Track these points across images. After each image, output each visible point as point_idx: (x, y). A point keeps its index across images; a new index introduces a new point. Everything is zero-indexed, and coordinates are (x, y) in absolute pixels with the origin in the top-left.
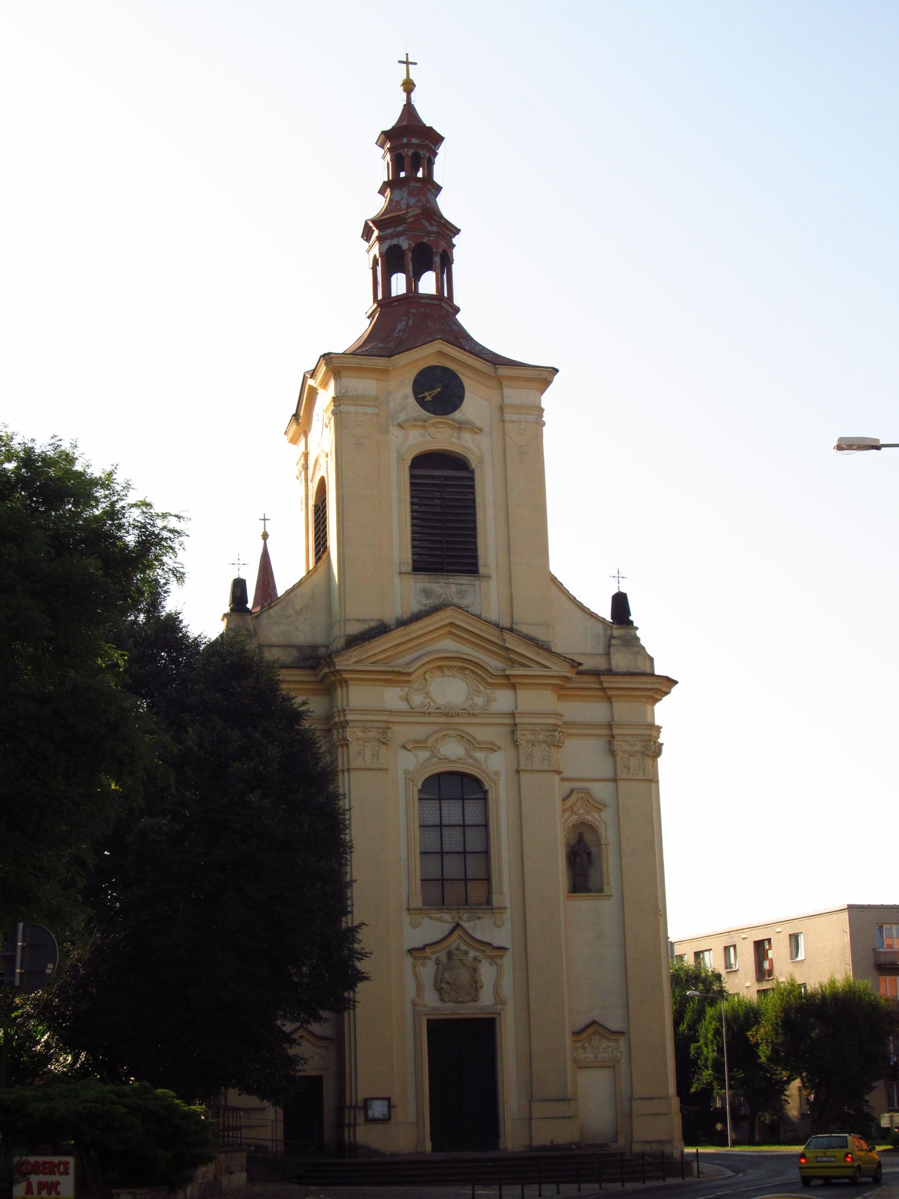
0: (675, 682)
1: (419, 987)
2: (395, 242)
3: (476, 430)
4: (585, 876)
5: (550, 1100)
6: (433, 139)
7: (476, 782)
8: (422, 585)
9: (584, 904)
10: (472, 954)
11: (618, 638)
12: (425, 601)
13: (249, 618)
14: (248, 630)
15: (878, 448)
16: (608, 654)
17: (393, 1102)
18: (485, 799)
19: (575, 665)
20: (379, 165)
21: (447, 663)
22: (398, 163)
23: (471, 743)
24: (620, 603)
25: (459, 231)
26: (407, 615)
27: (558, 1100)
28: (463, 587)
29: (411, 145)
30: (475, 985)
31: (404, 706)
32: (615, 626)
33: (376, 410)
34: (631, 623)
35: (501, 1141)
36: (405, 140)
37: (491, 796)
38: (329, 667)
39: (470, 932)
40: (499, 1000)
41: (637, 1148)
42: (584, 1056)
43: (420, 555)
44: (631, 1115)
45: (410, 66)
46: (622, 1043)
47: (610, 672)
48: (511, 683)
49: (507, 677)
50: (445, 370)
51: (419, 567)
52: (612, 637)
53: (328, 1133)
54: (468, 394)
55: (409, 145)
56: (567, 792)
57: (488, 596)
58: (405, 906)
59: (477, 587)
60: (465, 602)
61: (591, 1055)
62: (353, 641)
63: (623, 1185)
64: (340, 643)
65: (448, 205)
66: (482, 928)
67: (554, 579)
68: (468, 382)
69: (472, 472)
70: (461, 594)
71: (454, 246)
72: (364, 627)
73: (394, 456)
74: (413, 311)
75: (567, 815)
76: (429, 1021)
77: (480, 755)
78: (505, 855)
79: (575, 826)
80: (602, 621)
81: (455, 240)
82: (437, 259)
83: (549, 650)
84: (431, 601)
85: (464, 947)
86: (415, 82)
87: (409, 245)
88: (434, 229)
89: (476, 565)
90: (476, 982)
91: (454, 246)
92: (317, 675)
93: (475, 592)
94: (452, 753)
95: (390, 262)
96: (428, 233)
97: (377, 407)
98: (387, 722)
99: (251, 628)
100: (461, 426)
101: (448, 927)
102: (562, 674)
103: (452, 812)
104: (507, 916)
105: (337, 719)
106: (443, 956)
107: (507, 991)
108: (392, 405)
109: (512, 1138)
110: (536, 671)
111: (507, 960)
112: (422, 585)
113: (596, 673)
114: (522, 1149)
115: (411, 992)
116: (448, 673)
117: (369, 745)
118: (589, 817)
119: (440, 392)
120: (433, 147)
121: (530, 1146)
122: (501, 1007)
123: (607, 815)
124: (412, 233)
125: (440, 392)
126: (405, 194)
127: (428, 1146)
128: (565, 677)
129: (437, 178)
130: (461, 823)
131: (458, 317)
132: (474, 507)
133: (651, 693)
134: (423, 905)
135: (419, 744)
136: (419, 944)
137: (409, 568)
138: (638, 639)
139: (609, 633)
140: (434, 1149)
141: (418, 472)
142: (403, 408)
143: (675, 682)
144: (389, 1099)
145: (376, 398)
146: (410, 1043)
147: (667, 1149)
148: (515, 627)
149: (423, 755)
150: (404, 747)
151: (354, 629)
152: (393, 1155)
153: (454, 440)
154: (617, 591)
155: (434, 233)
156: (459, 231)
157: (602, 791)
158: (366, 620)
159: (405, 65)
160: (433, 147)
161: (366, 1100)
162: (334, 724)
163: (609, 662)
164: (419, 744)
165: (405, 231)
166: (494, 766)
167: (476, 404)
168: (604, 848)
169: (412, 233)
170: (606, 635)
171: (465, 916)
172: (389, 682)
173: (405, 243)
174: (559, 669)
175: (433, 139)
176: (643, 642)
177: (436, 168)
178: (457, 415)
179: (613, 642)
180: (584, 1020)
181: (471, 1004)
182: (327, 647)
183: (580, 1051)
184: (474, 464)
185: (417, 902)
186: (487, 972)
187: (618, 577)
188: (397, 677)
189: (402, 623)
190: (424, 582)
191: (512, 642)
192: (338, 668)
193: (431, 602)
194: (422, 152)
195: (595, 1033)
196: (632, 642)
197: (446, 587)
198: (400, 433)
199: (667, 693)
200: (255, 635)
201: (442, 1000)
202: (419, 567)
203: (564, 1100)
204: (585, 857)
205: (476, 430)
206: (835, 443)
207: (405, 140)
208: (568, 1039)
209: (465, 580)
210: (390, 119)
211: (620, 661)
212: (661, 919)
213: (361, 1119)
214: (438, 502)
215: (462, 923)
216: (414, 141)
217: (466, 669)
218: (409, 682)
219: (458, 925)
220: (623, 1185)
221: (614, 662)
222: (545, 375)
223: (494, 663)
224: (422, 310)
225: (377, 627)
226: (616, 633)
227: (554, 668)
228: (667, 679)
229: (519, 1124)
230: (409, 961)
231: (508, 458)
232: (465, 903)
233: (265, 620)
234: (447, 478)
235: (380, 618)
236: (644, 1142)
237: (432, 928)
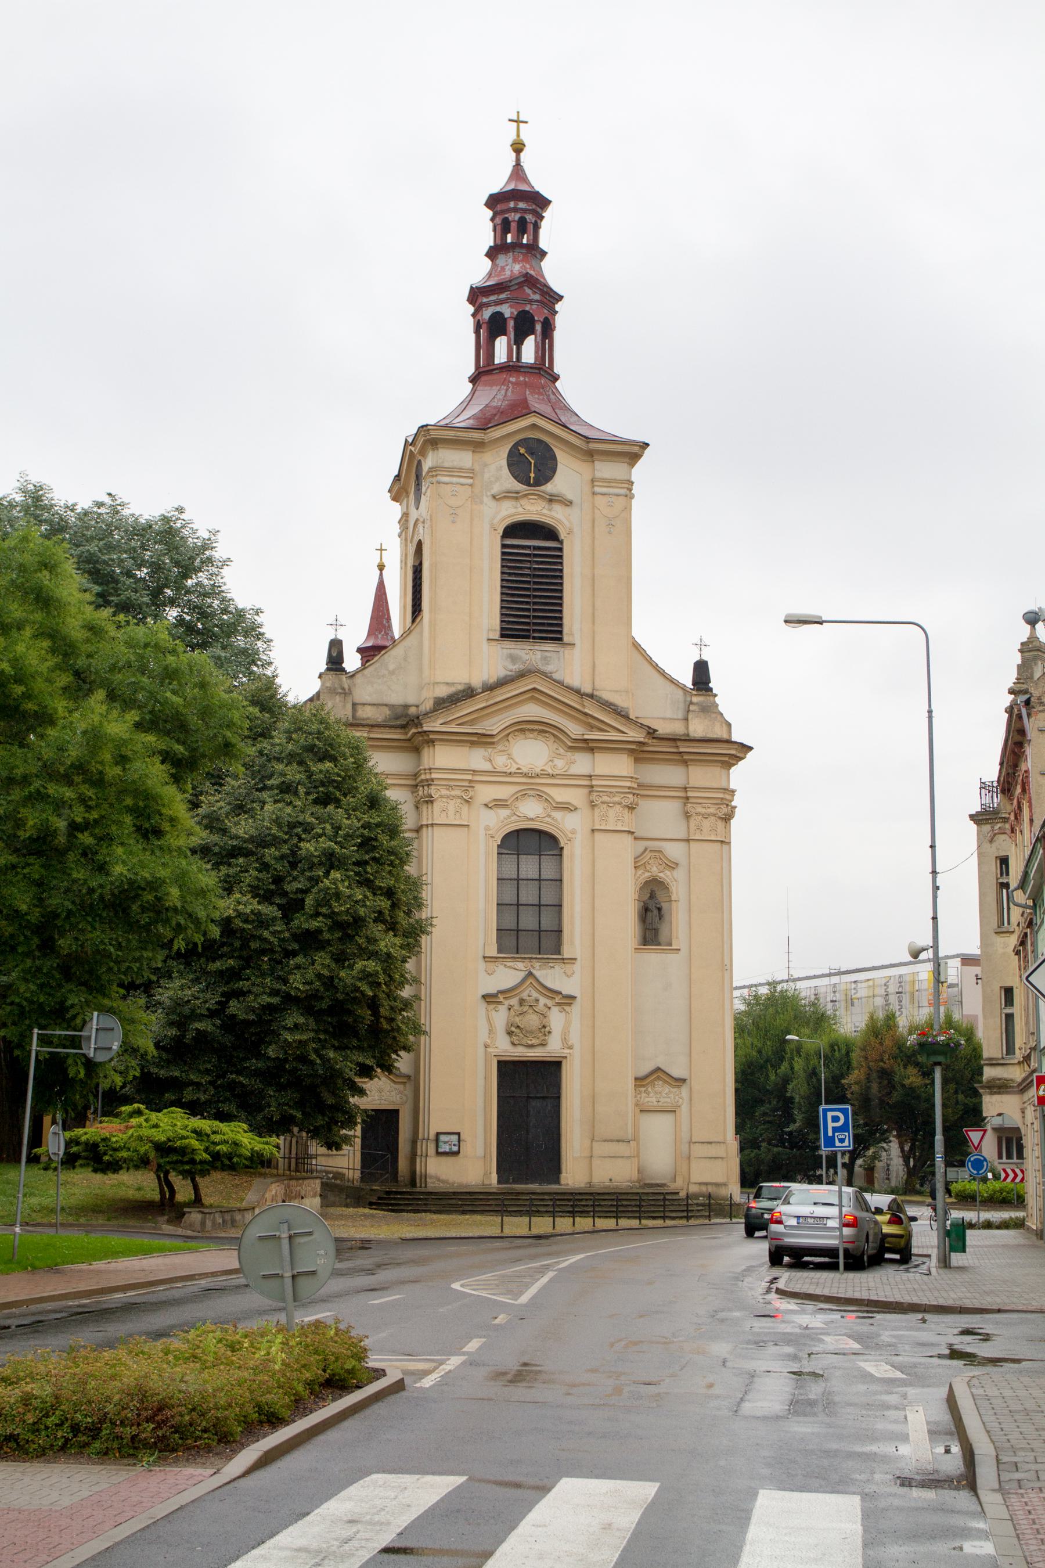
0: (751, 748)
1: (491, 1031)
2: (498, 309)
3: (569, 503)
4: (656, 931)
5: (612, 1141)
6: (540, 202)
7: (553, 839)
8: (509, 651)
10: (543, 1001)
11: (697, 704)
12: (511, 667)
13: (344, 677)
14: (343, 689)
15: (821, 623)
19: (651, 733)
20: (483, 232)
21: (528, 727)
22: (502, 227)
24: (701, 670)
25: (562, 297)
26: (493, 680)
27: (618, 1141)
28: (547, 654)
29: (517, 213)
30: (544, 1030)
31: (487, 766)
32: (695, 693)
33: (470, 481)
34: (711, 690)
35: (563, 1176)
36: (512, 205)
37: (565, 852)
38: (416, 727)
39: (541, 980)
41: (694, 1189)
42: (647, 1100)
44: (689, 1158)
45: (521, 125)
46: (684, 1091)
47: (688, 740)
48: (588, 746)
50: (540, 441)
51: (507, 634)
52: (691, 703)
53: (403, 1164)
54: (560, 467)
55: (515, 210)
56: (642, 849)
57: (571, 664)
58: (481, 955)
59: (561, 653)
60: (548, 668)
61: (654, 1100)
62: (443, 704)
64: (428, 705)
65: (553, 272)
66: (552, 976)
67: (636, 646)
68: (561, 456)
69: (561, 542)
71: (556, 312)
72: (452, 690)
73: (487, 527)
74: (513, 379)
75: (640, 872)
76: (499, 1062)
77: (558, 815)
78: (578, 908)
79: (647, 883)
80: (683, 688)
81: (558, 307)
82: (538, 327)
83: (626, 717)
84: (516, 666)
86: (526, 143)
87: (512, 313)
88: (537, 297)
91: (556, 312)
92: (406, 734)
93: (559, 659)
94: (532, 812)
95: (490, 328)
96: (531, 301)
97: (472, 478)
98: (470, 781)
99: (346, 687)
100: (552, 499)
101: (521, 975)
102: (637, 740)
103: (529, 867)
104: (577, 967)
105: (423, 777)
106: (514, 1002)
107: (574, 1039)
108: (486, 476)
109: (576, 1171)
110: (613, 736)
111: (576, 1009)
112: (509, 651)
113: (673, 740)
114: (583, 1185)
115: (483, 1036)
116: (531, 736)
117: (452, 802)
118: (661, 875)
119: (533, 463)
120: (539, 210)
121: (590, 1183)
122: (568, 1051)
123: (679, 874)
124: (515, 309)
125: (533, 463)
126: (510, 260)
127: (494, 1178)
128: (640, 743)
129: (543, 244)
130: (537, 877)
131: (558, 384)
133: (726, 759)
134: (500, 951)
135: (499, 804)
137: (497, 635)
138: (717, 705)
139: (689, 699)
140: (499, 1182)
141: (509, 542)
142: (497, 479)
143: (751, 748)
144: (459, 1134)
145: (472, 470)
146: (481, 1082)
148: (595, 693)
149: (504, 813)
151: (443, 692)
152: (461, 1185)
153: (545, 511)
154: (698, 659)
155: (537, 301)
156: (562, 297)
157: (674, 851)
158: (453, 684)
159: (515, 124)
160: (539, 210)
161: (438, 1134)
162: (418, 783)
163: (687, 728)
164: (499, 804)
165: (508, 298)
167: (570, 474)
168: (674, 904)
169: (515, 309)
170: (685, 701)
171: (537, 965)
172: (473, 744)
173: (507, 311)
174: (635, 735)
175: (540, 202)
176: (720, 708)
177: (543, 233)
178: (549, 487)
179: (692, 708)
180: (646, 1068)
182: (417, 706)
183: (644, 1095)
184: (562, 536)
185: (493, 951)
186: (556, 1019)
187: (701, 645)
188: (482, 740)
189: (490, 688)
190: (512, 647)
192: (425, 729)
193: (517, 667)
194: (529, 217)
195: (659, 1078)
196: (710, 710)
197: (532, 653)
198: (493, 504)
199: (741, 759)
200: (350, 693)
201: (513, 1044)
202: (507, 634)
203: (623, 1141)
204: (656, 912)
205: (569, 503)
206: (783, 618)
207: (512, 205)
208: (631, 1083)
209: (549, 647)
210: (499, 182)
211: (698, 728)
212: (727, 975)
213: (432, 1149)
215: (534, 972)
216: (522, 205)
217: (547, 732)
218: (493, 743)
219: (530, 974)
221: (691, 729)
222: (636, 449)
224: (522, 379)
225: (464, 691)
226: (695, 699)
227: (631, 734)
228: (742, 745)
230: (483, 1005)
231: (596, 529)
233: (359, 679)
234: (536, 548)
235: (467, 681)
236: (700, 1184)
237: (507, 976)
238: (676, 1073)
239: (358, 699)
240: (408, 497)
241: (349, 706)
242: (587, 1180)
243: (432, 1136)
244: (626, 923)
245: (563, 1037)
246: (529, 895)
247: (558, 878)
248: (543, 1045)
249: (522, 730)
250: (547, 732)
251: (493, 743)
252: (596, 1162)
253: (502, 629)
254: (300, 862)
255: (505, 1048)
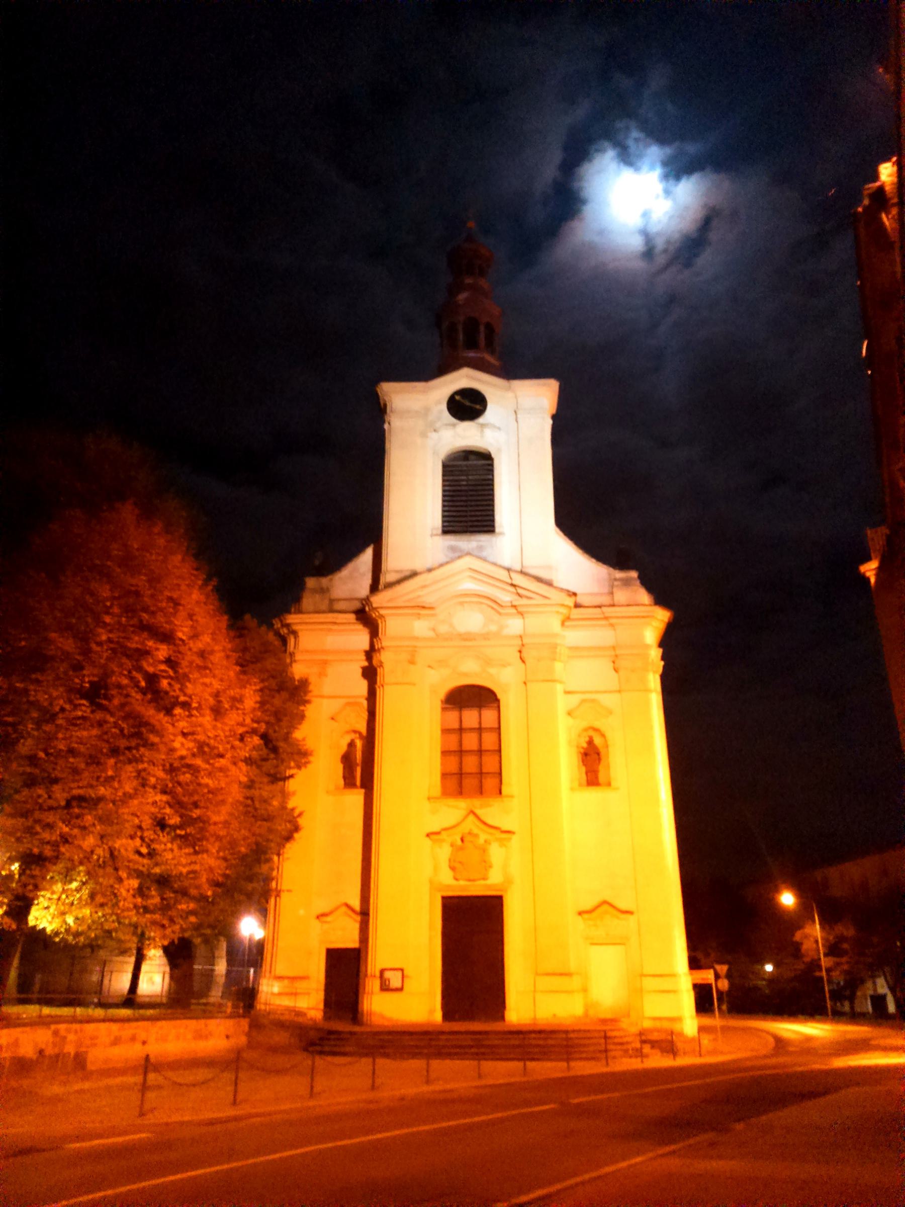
9: (593, 795)
16: (612, 593)
17: (405, 973)
18: (499, 707)
23: (488, 662)
30: (486, 865)
40: (508, 881)
43: (448, 522)
49: (515, 607)
51: (446, 531)
63: (642, 1062)
70: (481, 548)
85: (475, 831)
89: (493, 526)
90: (485, 862)
94: (471, 672)
101: (463, 813)
103: (470, 717)
121: (535, 1019)
127: (438, 1016)
132: (493, 485)
136: (436, 829)
137: (440, 531)
144: (402, 970)
147: (676, 1027)
150: (429, 667)
161: (382, 971)
166: (504, 679)
181: (482, 882)
186: (496, 853)
191: (518, 580)
202: (446, 531)
213: (377, 983)
214: (464, 483)
217: (481, 603)
218: (433, 615)
220: (642, 1062)
223: (506, 597)
229: (529, 998)
232: (480, 791)
238: (623, 906)
239: (332, 597)
240: (419, 596)
241: (327, 602)
242: (532, 1016)
243: (378, 974)
244: (567, 764)
245: (504, 871)
246: (470, 741)
247: (703, 1052)
248: (485, 879)
249: (462, 603)
250: (481, 603)
251: (500, 613)
252: (539, 996)
253: (443, 526)
254: (92, 852)
255: (446, 878)
